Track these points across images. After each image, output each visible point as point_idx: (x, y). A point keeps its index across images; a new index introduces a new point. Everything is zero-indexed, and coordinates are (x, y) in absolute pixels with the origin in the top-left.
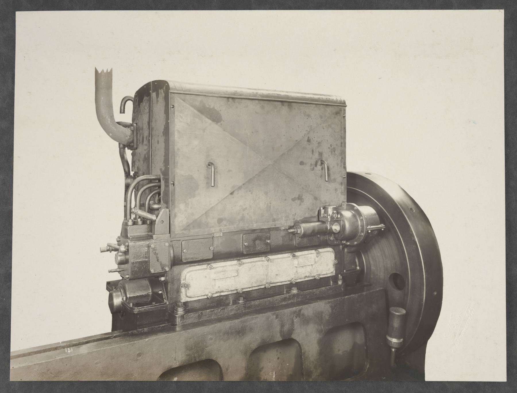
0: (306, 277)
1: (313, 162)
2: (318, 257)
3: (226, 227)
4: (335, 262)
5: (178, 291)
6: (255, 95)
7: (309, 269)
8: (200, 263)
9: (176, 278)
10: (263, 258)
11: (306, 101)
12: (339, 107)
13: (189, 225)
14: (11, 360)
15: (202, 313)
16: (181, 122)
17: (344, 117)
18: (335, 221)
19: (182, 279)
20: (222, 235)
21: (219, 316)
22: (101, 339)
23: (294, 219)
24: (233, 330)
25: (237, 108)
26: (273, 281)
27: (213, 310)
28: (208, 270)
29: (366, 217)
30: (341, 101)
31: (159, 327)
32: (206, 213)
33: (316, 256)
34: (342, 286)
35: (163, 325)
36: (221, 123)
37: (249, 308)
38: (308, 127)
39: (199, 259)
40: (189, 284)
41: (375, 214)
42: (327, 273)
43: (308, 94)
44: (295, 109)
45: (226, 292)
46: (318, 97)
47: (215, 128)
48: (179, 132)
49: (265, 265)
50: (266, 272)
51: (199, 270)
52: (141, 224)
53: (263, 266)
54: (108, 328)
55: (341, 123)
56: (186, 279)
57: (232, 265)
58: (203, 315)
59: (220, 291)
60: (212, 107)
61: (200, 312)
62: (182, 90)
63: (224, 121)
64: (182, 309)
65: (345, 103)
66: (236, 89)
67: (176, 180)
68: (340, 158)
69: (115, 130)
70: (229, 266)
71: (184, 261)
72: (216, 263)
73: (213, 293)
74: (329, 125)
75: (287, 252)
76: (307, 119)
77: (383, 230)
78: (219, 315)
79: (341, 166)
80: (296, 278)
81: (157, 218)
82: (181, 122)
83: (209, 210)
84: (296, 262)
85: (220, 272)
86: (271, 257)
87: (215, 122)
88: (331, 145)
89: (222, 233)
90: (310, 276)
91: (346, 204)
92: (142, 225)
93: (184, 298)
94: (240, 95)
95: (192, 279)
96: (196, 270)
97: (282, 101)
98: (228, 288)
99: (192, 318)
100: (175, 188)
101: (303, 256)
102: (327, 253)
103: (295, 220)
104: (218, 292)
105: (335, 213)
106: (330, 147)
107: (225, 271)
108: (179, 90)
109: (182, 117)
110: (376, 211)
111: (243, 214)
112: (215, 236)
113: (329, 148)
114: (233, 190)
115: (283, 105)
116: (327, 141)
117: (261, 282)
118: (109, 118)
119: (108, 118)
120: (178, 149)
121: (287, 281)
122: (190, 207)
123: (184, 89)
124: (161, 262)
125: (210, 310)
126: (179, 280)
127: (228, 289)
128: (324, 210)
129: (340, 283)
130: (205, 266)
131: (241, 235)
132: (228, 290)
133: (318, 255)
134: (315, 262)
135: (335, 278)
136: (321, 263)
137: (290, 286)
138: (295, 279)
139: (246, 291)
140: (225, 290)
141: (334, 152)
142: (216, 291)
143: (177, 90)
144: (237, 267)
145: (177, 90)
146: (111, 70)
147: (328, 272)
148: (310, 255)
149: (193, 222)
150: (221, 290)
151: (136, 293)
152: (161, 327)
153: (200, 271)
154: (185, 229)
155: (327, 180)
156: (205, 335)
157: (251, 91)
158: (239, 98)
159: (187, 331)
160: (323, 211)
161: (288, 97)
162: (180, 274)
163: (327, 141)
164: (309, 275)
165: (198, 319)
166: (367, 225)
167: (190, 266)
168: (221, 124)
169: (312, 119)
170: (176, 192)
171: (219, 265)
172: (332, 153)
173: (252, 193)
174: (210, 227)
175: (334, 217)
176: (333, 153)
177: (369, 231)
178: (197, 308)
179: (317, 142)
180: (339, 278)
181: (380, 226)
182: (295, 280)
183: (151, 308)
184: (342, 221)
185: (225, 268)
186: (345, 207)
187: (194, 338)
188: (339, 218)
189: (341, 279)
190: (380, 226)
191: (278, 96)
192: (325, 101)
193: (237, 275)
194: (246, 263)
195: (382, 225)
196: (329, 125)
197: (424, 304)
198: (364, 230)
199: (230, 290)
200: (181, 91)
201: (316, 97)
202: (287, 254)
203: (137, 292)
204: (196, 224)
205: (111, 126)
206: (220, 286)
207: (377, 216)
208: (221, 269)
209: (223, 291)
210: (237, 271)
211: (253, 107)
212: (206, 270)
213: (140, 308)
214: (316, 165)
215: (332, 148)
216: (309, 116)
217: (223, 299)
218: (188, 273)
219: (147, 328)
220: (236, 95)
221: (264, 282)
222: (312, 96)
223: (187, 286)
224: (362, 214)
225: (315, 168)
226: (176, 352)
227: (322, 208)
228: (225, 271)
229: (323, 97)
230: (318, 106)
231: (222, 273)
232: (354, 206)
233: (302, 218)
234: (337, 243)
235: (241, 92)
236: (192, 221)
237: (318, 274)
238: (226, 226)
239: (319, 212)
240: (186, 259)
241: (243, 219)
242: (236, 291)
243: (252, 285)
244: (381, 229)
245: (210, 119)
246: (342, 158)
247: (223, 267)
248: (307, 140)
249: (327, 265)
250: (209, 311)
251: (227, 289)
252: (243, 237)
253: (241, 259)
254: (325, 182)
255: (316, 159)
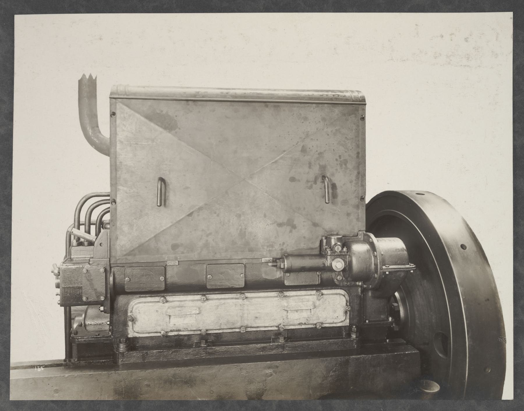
0: (300, 324)
1: (311, 177)
2: (319, 300)
3: (183, 255)
4: (347, 308)
5: (125, 325)
6: (225, 96)
7: (305, 314)
8: (159, 294)
9: (122, 309)
10: (238, 295)
11: (301, 100)
12: (354, 105)
13: (133, 250)
14: (11, 371)
15: (147, 353)
16: (123, 130)
17: (363, 119)
18: (337, 255)
19: (129, 311)
20: (178, 264)
21: (170, 359)
22: (51, 366)
23: (282, 249)
24: (177, 379)
25: (199, 112)
26: (250, 325)
27: (162, 351)
28: (161, 304)
29: (382, 253)
30: (352, 97)
31: (98, 362)
32: (155, 237)
33: (316, 299)
34: (355, 341)
35: (104, 361)
36: (176, 131)
37: (210, 354)
38: (304, 133)
39: (147, 290)
40: (136, 317)
41: (402, 250)
42: (334, 322)
43: (304, 91)
44: (284, 111)
45: (187, 332)
46: (321, 93)
47: (167, 136)
48: (121, 142)
49: (239, 304)
50: (241, 313)
51: (151, 302)
52: (76, 245)
53: (236, 305)
54: (60, 355)
55: (358, 126)
56: (133, 311)
57: (193, 301)
58: (148, 356)
59: (176, 329)
60: (164, 112)
61: (144, 351)
62: (126, 94)
63: (179, 129)
64: (124, 346)
65: (364, 100)
66: (198, 90)
67: (118, 198)
68: (355, 172)
69: (97, 141)
70: (190, 300)
71: (127, 291)
72: (174, 297)
73: (166, 330)
74: (336, 130)
75: (195, 294)
76: (303, 122)
77: (412, 273)
78: (170, 358)
79: (357, 183)
80: (284, 324)
81: (96, 240)
82: (123, 130)
83: (159, 234)
84: (284, 303)
85: (176, 307)
86: (248, 295)
87: (168, 130)
88: (340, 156)
89: (177, 262)
90: (306, 324)
91: (364, 233)
92: (88, 246)
93: (132, 332)
94: (203, 97)
95: (139, 313)
96: (145, 302)
97: (316, 102)
98: (187, 328)
99: (135, 357)
100: (116, 206)
101: (296, 298)
102: (335, 296)
103: (283, 251)
104: (174, 330)
105: (339, 245)
106: (338, 158)
107: (182, 307)
108: (121, 95)
109: (125, 126)
110: (406, 245)
111: (207, 241)
112: (168, 265)
113: (337, 160)
114: (191, 211)
115: (267, 106)
116: (334, 151)
117: (233, 324)
118: (90, 129)
119: (89, 129)
120: (121, 162)
121: (273, 326)
122: (134, 229)
123: (127, 94)
124: (95, 290)
125: (158, 351)
126: (126, 312)
127: (187, 329)
128: (326, 240)
129: (354, 336)
130: (157, 299)
131: (205, 266)
132: (186, 330)
133: (319, 298)
134: (315, 307)
135: (348, 329)
136: (325, 309)
137: (278, 334)
138: (284, 326)
139: (215, 333)
140: (183, 329)
141: (346, 165)
142: (171, 329)
143: (119, 95)
144: (199, 303)
145: (119, 95)
146: (96, 78)
147: (335, 321)
148: (307, 297)
149: (139, 246)
150: (178, 329)
151: (94, 320)
152: (100, 362)
153: (150, 304)
154: (128, 254)
155: (327, 202)
156: (140, 380)
157: (218, 91)
158: (162, 99)
159: (117, 372)
160: (325, 241)
161: (272, 96)
162: (128, 304)
163: (334, 151)
164: (306, 322)
165: (142, 360)
166: (383, 263)
167: (140, 297)
168: (176, 133)
169: (309, 123)
170: (118, 211)
171: (175, 299)
172: (341, 165)
173: (218, 215)
174: (162, 254)
175: (336, 250)
176: (344, 166)
177: (387, 273)
178: (149, 346)
179: (317, 153)
180: (353, 331)
181: (408, 266)
182: (283, 327)
183: (92, 339)
184: (348, 256)
185: (182, 303)
186: (361, 237)
187: (126, 382)
188: (344, 252)
189: (355, 332)
190: (408, 266)
191: (259, 96)
192: (331, 99)
193: (198, 312)
194: (212, 299)
195: (412, 266)
196: (336, 130)
197: (466, 383)
198: (378, 270)
199: (189, 329)
200: (124, 95)
201: (316, 94)
202: (274, 293)
203: (96, 319)
204: (142, 248)
205: (93, 138)
206: (176, 324)
207: (406, 253)
208: (177, 304)
209: (180, 330)
210: (199, 308)
211: (221, 110)
212: (159, 304)
213: (80, 339)
214: (315, 182)
215: (341, 159)
216: (306, 119)
217: (183, 340)
218: (135, 304)
219: (84, 362)
220: (197, 96)
221: (238, 325)
222: (310, 93)
223: (133, 320)
224: (377, 248)
225: (314, 186)
226: (102, 395)
227: (324, 238)
228: (182, 307)
229: (330, 93)
230: (320, 105)
231: (179, 309)
232: (370, 237)
233: (294, 249)
234: (348, 284)
235: (205, 92)
236: (137, 246)
237: (320, 322)
238: (183, 253)
239: (321, 241)
240: (212, 285)
241: (206, 245)
242: (200, 331)
243: (220, 326)
244: (386, 272)
245: (161, 127)
246: (359, 173)
247: (181, 301)
248: (300, 150)
249: (335, 311)
250: (156, 352)
251: (186, 328)
252: (206, 267)
253: (284, 291)
254: (326, 204)
255: (316, 175)
